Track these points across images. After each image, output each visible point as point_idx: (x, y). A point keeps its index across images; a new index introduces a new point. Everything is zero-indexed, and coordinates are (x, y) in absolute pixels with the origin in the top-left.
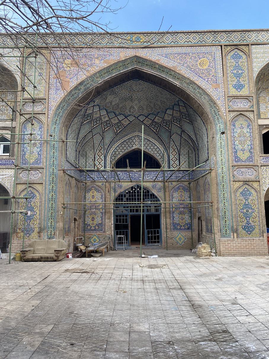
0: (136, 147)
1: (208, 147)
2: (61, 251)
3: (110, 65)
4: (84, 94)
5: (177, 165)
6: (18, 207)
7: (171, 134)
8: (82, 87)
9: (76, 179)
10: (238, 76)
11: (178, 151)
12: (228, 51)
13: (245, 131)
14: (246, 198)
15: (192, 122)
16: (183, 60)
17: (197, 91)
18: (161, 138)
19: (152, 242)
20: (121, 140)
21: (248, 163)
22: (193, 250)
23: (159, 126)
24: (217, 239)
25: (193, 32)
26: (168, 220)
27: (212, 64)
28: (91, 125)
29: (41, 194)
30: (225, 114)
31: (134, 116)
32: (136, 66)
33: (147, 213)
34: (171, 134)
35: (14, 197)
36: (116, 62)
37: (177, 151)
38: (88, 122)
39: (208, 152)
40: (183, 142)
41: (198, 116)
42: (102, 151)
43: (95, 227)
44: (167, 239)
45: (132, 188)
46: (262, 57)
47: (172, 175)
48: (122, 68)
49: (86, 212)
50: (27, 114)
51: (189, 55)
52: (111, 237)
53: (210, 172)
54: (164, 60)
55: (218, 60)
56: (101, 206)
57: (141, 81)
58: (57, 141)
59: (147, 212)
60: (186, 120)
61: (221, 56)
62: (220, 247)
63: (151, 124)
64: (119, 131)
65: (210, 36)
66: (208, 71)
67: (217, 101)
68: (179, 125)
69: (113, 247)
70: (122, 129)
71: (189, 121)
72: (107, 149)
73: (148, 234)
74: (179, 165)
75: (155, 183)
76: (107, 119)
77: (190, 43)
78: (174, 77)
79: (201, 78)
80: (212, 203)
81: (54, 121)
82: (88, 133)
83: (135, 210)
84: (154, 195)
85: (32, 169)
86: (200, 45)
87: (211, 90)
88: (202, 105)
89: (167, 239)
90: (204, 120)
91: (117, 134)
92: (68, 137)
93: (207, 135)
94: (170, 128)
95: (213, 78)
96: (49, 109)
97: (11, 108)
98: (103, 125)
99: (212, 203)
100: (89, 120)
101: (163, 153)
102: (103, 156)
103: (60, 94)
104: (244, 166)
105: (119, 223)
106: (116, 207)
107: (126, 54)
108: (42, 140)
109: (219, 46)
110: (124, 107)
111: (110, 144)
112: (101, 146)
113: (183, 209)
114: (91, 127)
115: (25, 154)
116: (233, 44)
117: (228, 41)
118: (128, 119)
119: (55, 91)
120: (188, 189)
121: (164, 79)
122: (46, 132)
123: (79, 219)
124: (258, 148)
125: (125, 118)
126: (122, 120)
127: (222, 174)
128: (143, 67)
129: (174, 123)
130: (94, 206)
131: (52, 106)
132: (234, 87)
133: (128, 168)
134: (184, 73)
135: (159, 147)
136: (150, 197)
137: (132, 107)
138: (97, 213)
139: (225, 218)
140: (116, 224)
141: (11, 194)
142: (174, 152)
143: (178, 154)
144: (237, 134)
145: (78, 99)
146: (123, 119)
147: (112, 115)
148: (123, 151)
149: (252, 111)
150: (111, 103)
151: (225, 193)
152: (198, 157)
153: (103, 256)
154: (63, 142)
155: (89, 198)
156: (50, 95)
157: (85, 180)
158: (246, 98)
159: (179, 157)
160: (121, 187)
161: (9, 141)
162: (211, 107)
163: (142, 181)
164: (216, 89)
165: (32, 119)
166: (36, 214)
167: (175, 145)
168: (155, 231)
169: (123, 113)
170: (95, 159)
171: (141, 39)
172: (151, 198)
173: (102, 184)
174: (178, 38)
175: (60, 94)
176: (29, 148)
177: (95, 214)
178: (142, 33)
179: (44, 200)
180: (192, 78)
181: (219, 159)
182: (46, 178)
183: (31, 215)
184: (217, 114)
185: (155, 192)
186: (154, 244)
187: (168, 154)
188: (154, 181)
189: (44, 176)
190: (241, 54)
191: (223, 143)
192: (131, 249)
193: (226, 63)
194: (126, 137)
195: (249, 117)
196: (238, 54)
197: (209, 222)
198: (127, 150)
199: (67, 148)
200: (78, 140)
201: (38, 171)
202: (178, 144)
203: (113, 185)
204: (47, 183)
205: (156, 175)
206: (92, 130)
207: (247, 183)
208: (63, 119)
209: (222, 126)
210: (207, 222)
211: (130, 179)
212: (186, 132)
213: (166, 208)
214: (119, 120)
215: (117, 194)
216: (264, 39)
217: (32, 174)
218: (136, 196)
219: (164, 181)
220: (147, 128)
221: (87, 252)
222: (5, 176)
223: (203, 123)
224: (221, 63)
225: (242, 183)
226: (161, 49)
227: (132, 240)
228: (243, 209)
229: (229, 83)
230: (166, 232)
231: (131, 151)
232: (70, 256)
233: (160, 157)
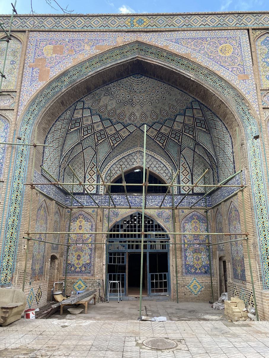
2: (12, 308)
3: (104, 51)
4: (69, 88)
7: (181, 148)
11: (190, 170)
15: (209, 131)
16: (198, 46)
17: (217, 84)
19: (157, 291)
20: (119, 156)
22: (214, 304)
23: (166, 138)
24: (257, 292)
25: (211, 14)
26: (179, 260)
27: (237, 51)
28: (80, 134)
30: (258, 113)
31: (135, 126)
32: (137, 56)
33: (152, 251)
34: (181, 148)
36: (112, 48)
37: (189, 170)
38: (76, 130)
39: (234, 166)
40: (197, 158)
41: (218, 120)
43: (80, 268)
44: (177, 287)
45: (132, 216)
48: (119, 57)
51: (206, 40)
52: (102, 283)
54: (174, 46)
55: (245, 46)
56: (90, 240)
57: (144, 77)
59: (151, 249)
60: (201, 128)
61: (248, 42)
62: (263, 304)
63: (157, 136)
64: (117, 144)
65: (233, 18)
66: (233, 58)
67: (247, 95)
68: (191, 137)
69: (103, 296)
70: (120, 142)
72: (101, 166)
73: (152, 279)
75: (161, 210)
76: (101, 128)
77: (207, 26)
78: (187, 67)
79: (222, 68)
80: (247, 236)
82: (76, 145)
83: (134, 247)
86: (220, 29)
88: (225, 103)
89: (177, 287)
90: (227, 124)
91: (113, 148)
93: (232, 144)
95: (239, 67)
96: (20, 104)
98: (95, 136)
99: (247, 236)
100: (77, 128)
101: (171, 172)
102: (95, 176)
103: (36, 85)
105: (113, 264)
107: (124, 39)
109: (245, 30)
110: (123, 113)
111: (104, 160)
112: (93, 163)
114: (80, 138)
116: (264, 27)
117: (257, 24)
118: (127, 129)
119: (30, 83)
120: (205, 220)
121: (174, 70)
122: (13, 133)
123: (60, 257)
125: (123, 128)
126: (120, 130)
128: (147, 56)
129: (186, 134)
130: (81, 239)
131: (24, 100)
133: (124, 183)
134: (200, 61)
135: (166, 165)
136: (154, 229)
137: (133, 114)
138: (84, 249)
140: (109, 265)
142: (185, 171)
143: (190, 174)
145: (61, 94)
147: (107, 123)
150: (106, 107)
151: (265, 221)
152: (218, 176)
153: (86, 313)
155: (75, 229)
156: (22, 87)
159: (192, 177)
160: (117, 215)
162: (238, 103)
164: (245, 81)
167: (187, 162)
168: (161, 275)
170: (85, 179)
171: (144, 22)
173: (93, 211)
174: (191, 21)
175: (36, 85)
178: (146, 15)
180: (211, 67)
182: (5, 196)
184: (247, 113)
185: (161, 222)
186: (159, 293)
188: (160, 208)
189: (3, 193)
192: (128, 300)
193: (256, 50)
194: (125, 153)
197: (238, 264)
198: (125, 169)
199: (45, 159)
202: (190, 161)
203: (106, 212)
204: (6, 203)
208: (38, 119)
210: (234, 265)
211: (129, 204)
212: (201, 144)
213: (175, 244)
214: (117, 130)
215: (111, 224)
218: (165, 280)
220: (151, 141)
221: (62, 307)
224: (249, 50)
226: (170, 33)
227: (129, 285)
229: (261, 74)
230: (177, 277)
232: (32, 315)
233: (167, 178)
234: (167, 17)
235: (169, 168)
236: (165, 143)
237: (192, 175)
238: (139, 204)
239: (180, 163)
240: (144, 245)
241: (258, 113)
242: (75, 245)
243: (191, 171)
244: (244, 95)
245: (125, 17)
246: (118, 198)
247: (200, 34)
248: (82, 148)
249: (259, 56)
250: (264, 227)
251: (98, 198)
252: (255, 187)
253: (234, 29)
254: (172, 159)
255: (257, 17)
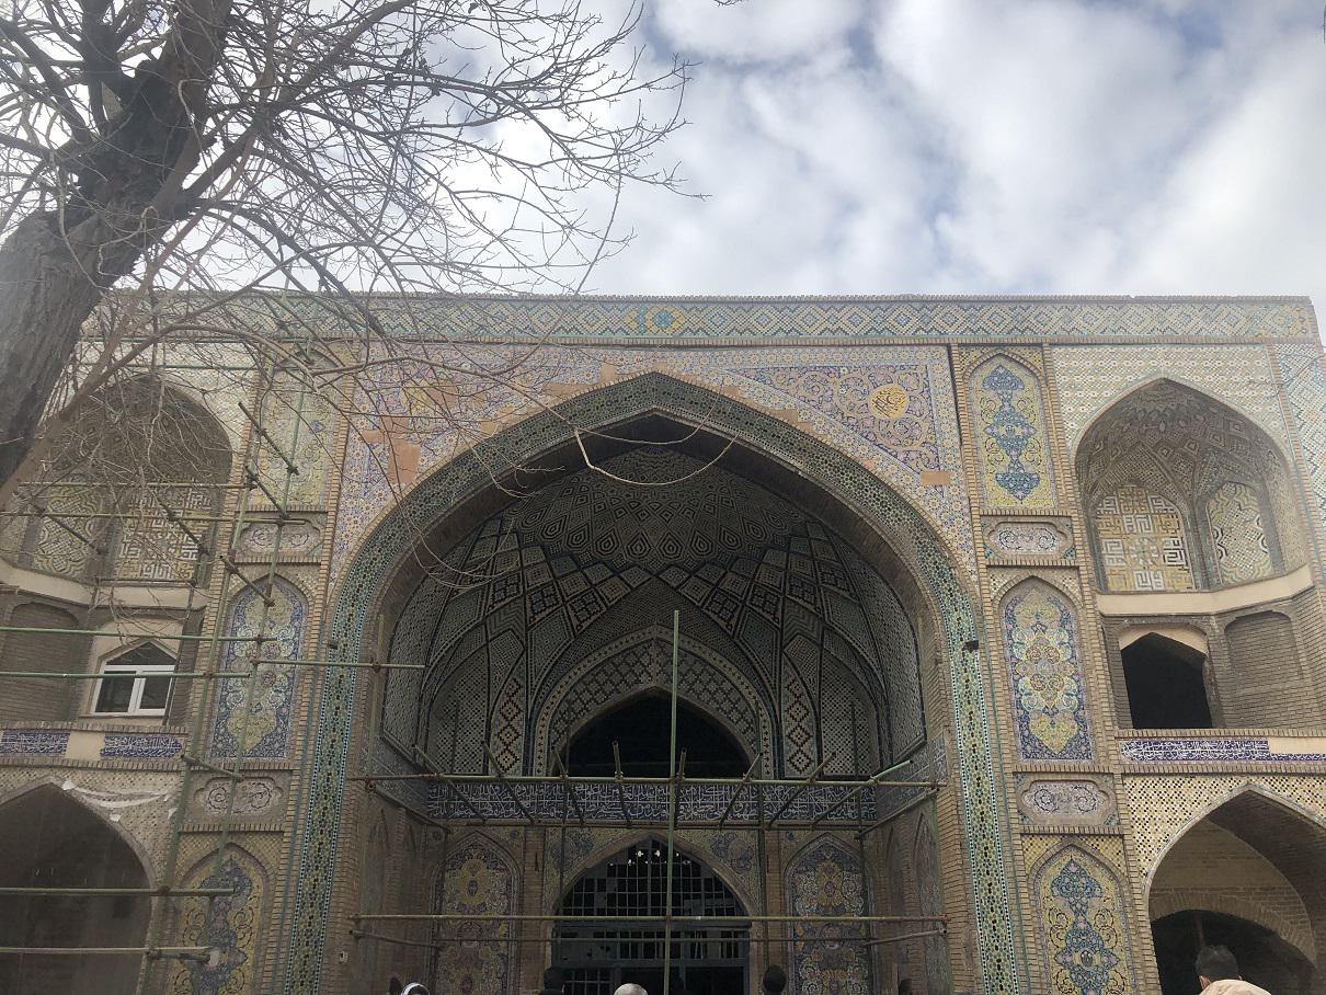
0: (653, 684)
1: (921, 694)
4: (470, 494)
5: (811, 761)
6: (175, 930)
7: (782, 638)
8: (464, 475)
9: (409, 813)
10: (1014, 445)
12: (971, 363)
13: (1054, 642)
14: (1078, 906)
18: (744, 649)
20: (596, 655)
21: (1072, 762)
23: (738, 606)
25: (850, 302)
29: (272, 877)
30: (974, 578)
34: (782, 638)
35: (164, 892)
37: (808, 704)
38: (473, 590)
42: (519, 699)
45: (632, 851)
46: (1092, 386)
47: (792, 799)
49: (441, 953)
50: (252, 564)
53: (933, 798)
58: (355, 667)
59: (693, 956)
67: (945, 529)
68: (811, 608)
71: (846, 595)
72: (539, 690)
74: (820, 762)
76: (546, 578)
77: (840, 335)
78: (788, 445)
79: (881, 451)
81: (351, 590)
82: (469, 631)
83: (641, 950)
84: (718, 883)
85: (247, 773)
87: (921, 491)
88: (889, 543)
92: (395, 645)
94: (779, 615)
95: (924, 450)
96: (336, 549)
97: (194, 539)
100: (476, 585)
104: (1060, 773)
106: (564, 932)
108: (298, 660)
111: (551, 671)
113: (837, 946)
115: (227, 715)
116: (989, 341)
120: (856, 861)
124: (1107, 705)
125: (610, 577)
126: (600, 582)
127: (979, 806)
131: (347, 536)
132: (1003, 481)
135: (738, 683)
136: (703, 892)
139: (1001, 987)
141: (155, 875)
143: (811, 715)
144: (1024, 652)
146: (605, 580)
148: (600, 697)
149: (1071, 567)
151: (993, 882)
154: (377, 669)
156: (343, 499)
157: (445, 816)
158: (1048, 521)
159: (818, 725)
160: (587, 846)
161: (167, 660)
162: (924, 548)
163: (671, 821)
164: (939, 489)
165: (270, 583)
166: (241, 960)
167: (801, 679)
169: (605, 559)
172: (708, 897)
173: (513, 835)
176: (244, 692)
177: (478, 964)
178: (680, 302)
179: (281, 899)
180: (850, 450)
181: (963, 746)
183: (223, 965)
187: (775, 716)
188: (722, 825)
190: (1019, 373)
191: (975, 685)
195: (1065, 591)
196: (1007, 373)
200: (431, 660)
201: (269, 784)
203: (554, 837)
205: (729, 801)
206: (486, 617)
207: (1077, 841)
209: (967, 623)
211: (625, 813)
215: (570, 877)
216: (1092, 329)
217: (245, 795)
218: (649, 887)
219: (758, 826)
222: (138, 802)
223: (899, 603)
224: (952, 402)
225: (1056, 840)
228: (1068, 951)
231: (629, 699)
233: (743, 725)
234: (735, 307)
235: (747, 696)
236: (735, 619)
237: (816, 719)
238: (656, 812)
239: (780, 682)
240: (672, 944)
241: (974, 578)
242: (457, 944)
243: (813, 706)
244: (936, 529)
245: (621, 306)
246: (589, 793)
247: (821, 357)
248: (487, 636)
249: (977, 419)
250: (991, 900)
251: (528, 791)
252: (970, 785)
253: (911, 345)
254: (757, 666)
255: (972, 311)
